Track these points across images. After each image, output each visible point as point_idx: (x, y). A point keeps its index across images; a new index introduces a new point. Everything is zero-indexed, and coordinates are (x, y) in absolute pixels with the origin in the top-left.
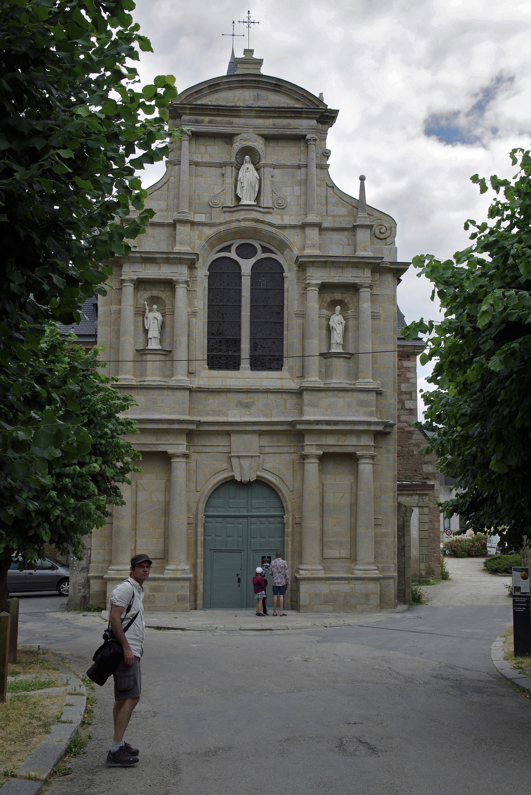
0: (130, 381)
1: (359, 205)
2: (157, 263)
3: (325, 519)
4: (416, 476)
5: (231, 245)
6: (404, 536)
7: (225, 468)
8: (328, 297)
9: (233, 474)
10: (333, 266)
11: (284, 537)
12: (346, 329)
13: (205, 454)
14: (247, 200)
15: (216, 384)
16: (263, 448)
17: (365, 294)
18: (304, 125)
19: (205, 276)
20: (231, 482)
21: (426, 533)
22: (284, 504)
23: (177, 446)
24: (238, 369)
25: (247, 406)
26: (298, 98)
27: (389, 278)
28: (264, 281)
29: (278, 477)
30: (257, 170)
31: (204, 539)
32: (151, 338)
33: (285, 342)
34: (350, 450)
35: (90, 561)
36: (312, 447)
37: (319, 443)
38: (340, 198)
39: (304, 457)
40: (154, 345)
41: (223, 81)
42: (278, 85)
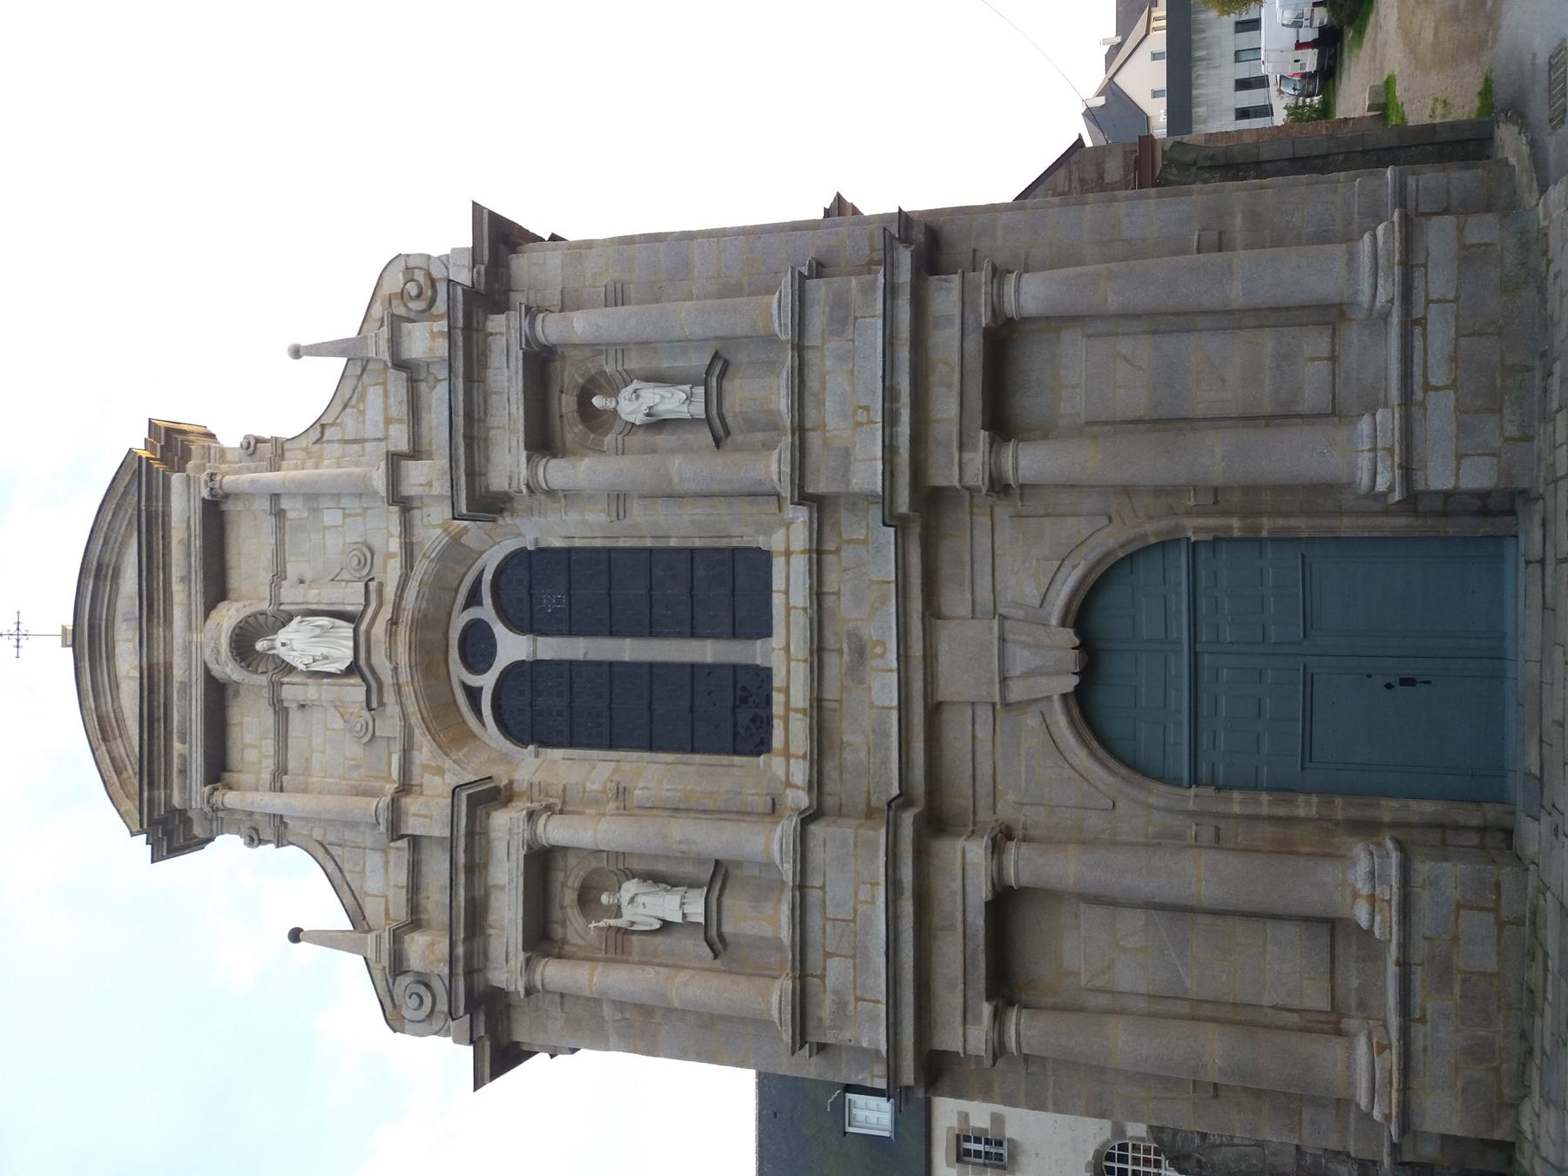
2: (487, 895)
3: (1200, 411)
5: (465, 687)
7: (1039, 719)
8: (572, 431)
9: (1056, 697)
11: (1261, 540)
12: (658, 378)
13: (999, 777)
16: (978, 607)
17: (551, 329)
18: (182, 510)
22: (1153, 540)
23: (967, 866)
25: (860, 651)
27: (522, 264)
30: (285, 619)
31: (1269, 790)
32: (684, 916)
33: (698, 543)
34: (975, 344)
36: (962, 463)
38: (345, 407)
39: (999, 487)
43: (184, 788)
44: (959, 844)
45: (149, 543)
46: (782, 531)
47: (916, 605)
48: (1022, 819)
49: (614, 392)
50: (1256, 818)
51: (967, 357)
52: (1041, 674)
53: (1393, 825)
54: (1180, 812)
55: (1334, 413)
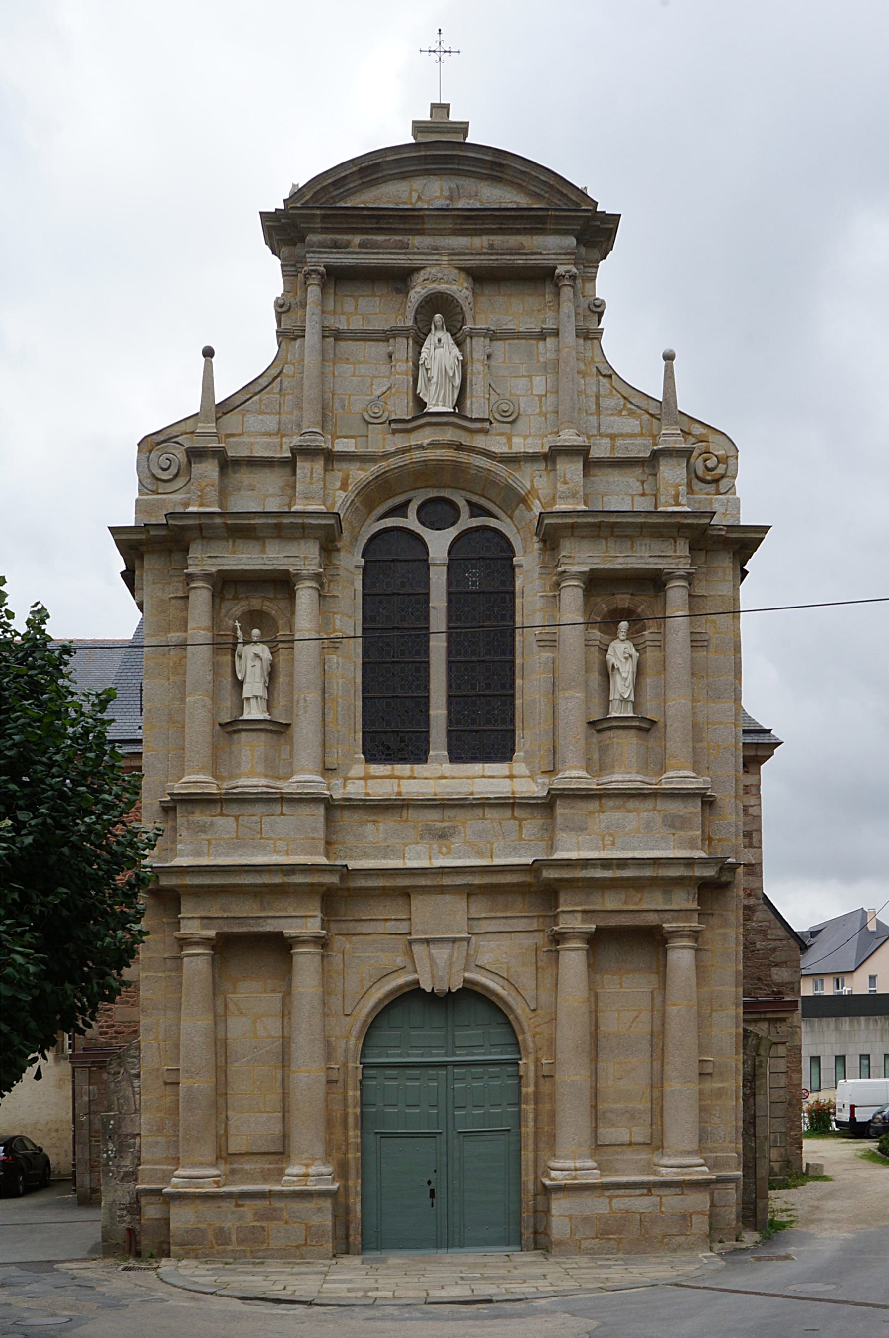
0: (207, 787)
1: (664, 410)
2: (257, 538)
3: (600, 1065)
4: (761, 989)
5: (407, 503)
6: (754, 1095)
8: (603, 605)
9: (416, 976)
10: (612, 535)
11: (518, 1104)
13: (361, 937)
14: (439, 402)
15: (381, 790)
16: (475, 922)
17: (677, 594)
18: (550, 248)
19: (357, 567)
20: (412, 996)
21: (782, 1092)
22: (520, 1038)
23: (302, 922)
24: (426, 761)
25: (443, 835)
26: (538, 191)
27: (725, 563)
28: (474, 575)
29: (506, 982)
30: (459, 344)
31: (362, 1112)
32: (248, 699)
33: (518, 702)
34: (652, 919)
35: (139, 1159)
37: (587, 908)
38: (625, 398)
39: (558, 938)
40: (254, 712)
41: (388, 159)
42: (499, 165)
43: (322, 245)
44: (318, 913)
45: (521, 217)
46: (528, 773)
47: (477, 880)
48: (334, 954)
49: (631, 636)
50: (346, 1106)
51: (644, 914)
52: (431, 966)
53: (346, 1188)
54: (346, 1057)
55: (598, 1147)
